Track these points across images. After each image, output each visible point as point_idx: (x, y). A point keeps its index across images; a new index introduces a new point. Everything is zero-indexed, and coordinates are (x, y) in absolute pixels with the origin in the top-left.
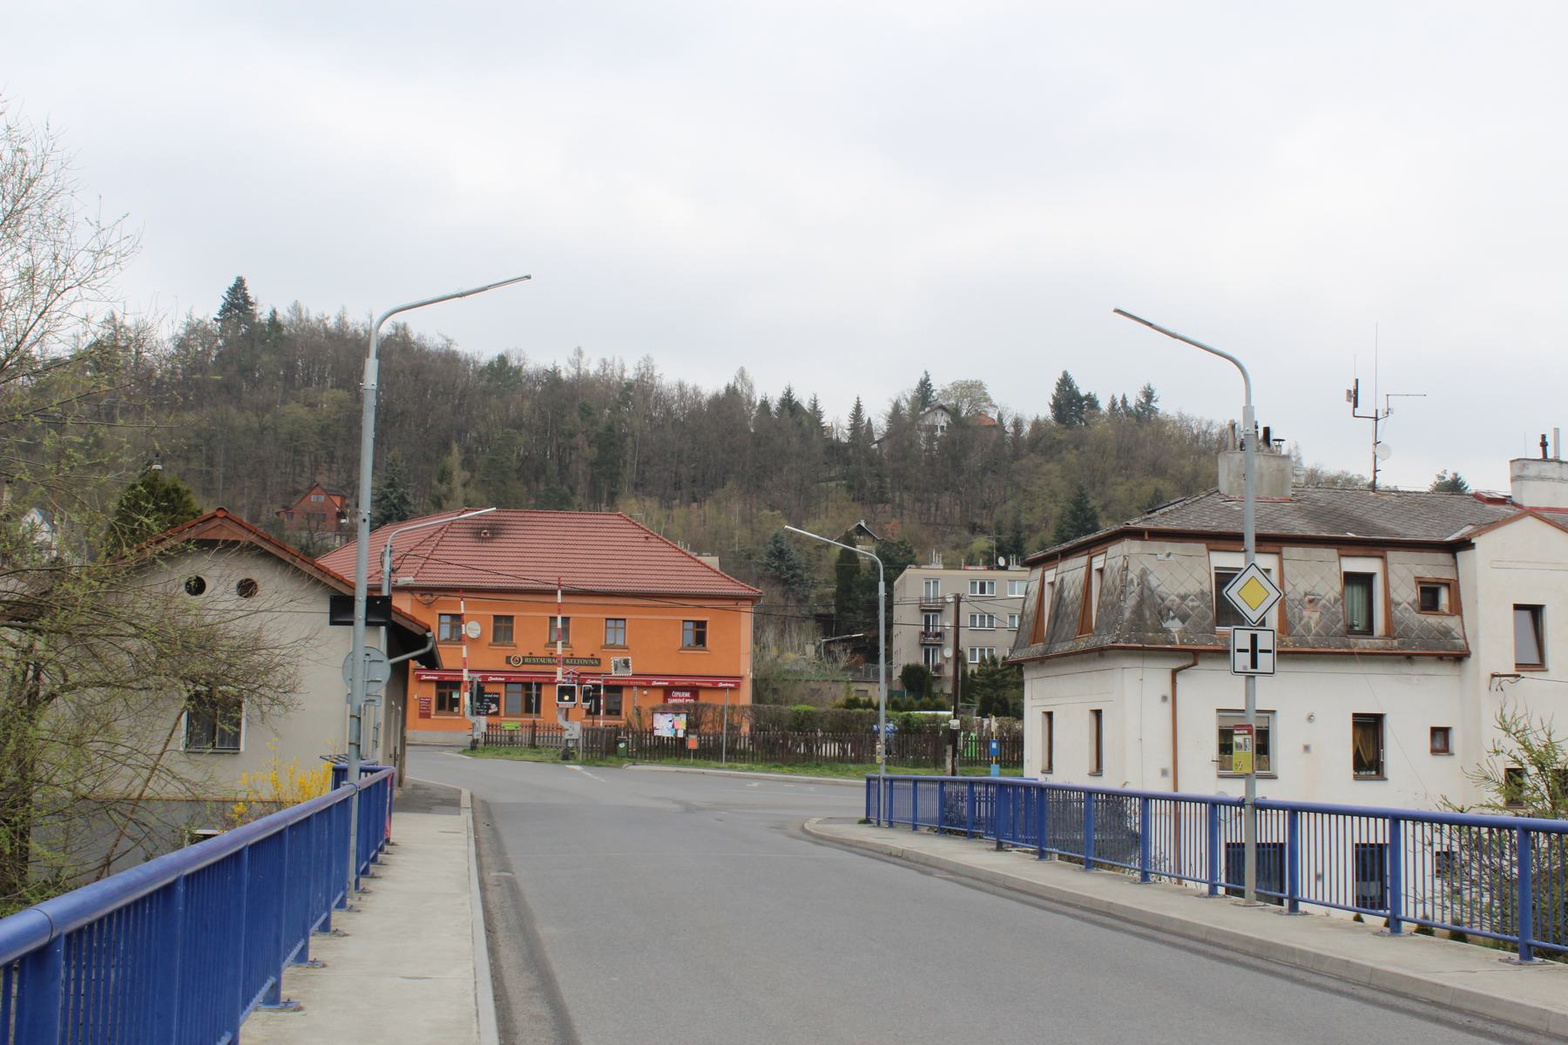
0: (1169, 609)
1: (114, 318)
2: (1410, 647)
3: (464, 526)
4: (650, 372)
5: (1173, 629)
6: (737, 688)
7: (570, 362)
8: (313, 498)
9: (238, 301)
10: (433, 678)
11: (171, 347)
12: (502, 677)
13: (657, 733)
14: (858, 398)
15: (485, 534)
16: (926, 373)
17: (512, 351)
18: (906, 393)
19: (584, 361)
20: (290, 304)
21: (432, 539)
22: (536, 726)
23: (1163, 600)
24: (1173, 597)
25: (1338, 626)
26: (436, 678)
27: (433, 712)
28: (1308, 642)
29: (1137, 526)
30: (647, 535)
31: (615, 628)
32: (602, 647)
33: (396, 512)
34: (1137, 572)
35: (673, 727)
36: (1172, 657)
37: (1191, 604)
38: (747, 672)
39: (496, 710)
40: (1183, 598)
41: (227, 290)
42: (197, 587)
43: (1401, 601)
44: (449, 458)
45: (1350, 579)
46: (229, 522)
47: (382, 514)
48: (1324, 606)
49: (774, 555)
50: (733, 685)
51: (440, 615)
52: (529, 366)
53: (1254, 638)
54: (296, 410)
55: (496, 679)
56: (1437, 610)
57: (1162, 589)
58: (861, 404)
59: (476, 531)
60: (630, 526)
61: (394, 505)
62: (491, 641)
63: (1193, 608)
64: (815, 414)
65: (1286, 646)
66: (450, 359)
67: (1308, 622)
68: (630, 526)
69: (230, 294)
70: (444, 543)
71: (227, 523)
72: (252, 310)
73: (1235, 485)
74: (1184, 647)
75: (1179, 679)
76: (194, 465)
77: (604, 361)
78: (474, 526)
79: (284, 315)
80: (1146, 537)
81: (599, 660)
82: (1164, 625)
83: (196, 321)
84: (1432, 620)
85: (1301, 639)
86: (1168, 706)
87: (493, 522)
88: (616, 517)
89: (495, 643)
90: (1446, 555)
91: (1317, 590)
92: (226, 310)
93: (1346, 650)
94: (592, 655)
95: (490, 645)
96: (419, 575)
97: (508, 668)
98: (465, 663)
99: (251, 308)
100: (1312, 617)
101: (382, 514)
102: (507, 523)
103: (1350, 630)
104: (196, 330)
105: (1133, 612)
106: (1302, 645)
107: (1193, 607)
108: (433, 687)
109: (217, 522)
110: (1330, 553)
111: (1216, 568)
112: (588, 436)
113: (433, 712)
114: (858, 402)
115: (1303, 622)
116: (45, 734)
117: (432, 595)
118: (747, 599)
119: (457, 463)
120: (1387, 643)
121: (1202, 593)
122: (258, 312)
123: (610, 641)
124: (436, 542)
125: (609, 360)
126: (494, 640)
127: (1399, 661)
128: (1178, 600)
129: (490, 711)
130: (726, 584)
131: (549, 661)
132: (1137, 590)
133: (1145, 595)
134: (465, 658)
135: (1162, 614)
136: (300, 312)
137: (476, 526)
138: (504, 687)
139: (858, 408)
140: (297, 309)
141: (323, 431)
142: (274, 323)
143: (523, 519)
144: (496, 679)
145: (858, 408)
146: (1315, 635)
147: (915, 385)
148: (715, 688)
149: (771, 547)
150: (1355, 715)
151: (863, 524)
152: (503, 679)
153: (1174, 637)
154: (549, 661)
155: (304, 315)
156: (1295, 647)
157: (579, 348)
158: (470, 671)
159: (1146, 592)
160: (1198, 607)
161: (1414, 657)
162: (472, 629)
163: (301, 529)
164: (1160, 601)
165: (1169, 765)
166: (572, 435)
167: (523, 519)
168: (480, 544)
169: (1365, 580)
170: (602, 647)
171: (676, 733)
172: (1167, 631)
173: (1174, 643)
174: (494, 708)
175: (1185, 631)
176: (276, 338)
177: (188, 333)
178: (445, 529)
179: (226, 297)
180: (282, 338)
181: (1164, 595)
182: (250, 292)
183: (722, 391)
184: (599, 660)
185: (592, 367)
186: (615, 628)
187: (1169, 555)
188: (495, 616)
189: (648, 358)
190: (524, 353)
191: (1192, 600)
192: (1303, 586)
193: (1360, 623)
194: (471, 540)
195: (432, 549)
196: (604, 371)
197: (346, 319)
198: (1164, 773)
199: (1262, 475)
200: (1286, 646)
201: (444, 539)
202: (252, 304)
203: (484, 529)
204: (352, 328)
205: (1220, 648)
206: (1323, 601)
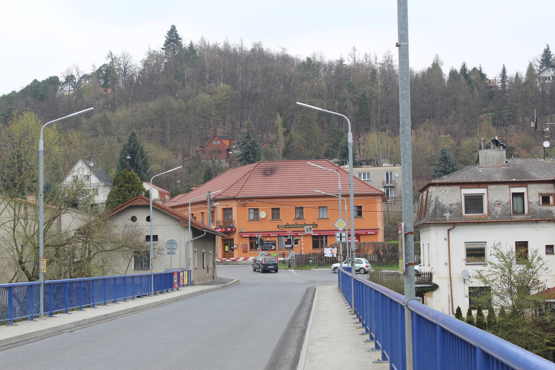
0: (446, 209)
1: (111, 54)
2: (535, 217)
3: (259, 170)
4: (390, 59)
5: (447, 216)
6: (376, 234)
7: (350, 55)
8: (214, 143)
10: (248, 236)
11: (141, 66)
12: (276, 234)
13: (325, 255)
14: (504, 65)
15: (268, 172)
16: (547, 45)
18: (538, 57)
19: (357, 54)
20: (199, 39)
21: (246, 176)
22: (285, 255)
23: (443, 206)
24: (447, 205)
26: (249, 236)
27: (248, 250)
28: (496, 218)
29: (435, 182)
30: (337, 169)
31: (323, 211)
32: (318, 219)
33: (251, 150)
34: (435, 197)
35: (332, 253)
36: (448, 225)
37: (453, 207)
38: (380, 226)
40: (451, 205)
41: (167, 32)
42: (134, 219)
43: (532, 202)
44: (276, 121)
45: (514, 195)
46: (142, 199)
47: (244, 152)
48: (503, 205)
49: (443, 160)
50: (374, 233)
51: (249, 209)
52: (326, 60)
54: (204, 97)
55: (274, 235)
56: (549, 204)
58: (506, 68)
59: (264, 171)
60: (331, 165)
61: (250, 147)
62: (271, 219)
63: (454, 209)
64: (483, 76)
65: (488, 220)
66: (285, 59)
68: (331, 165)
69: (168, 34)
70: (250, 178)
71: (142, 200)
72: (180, 42)
73: (484, 162)
74: (450, 222)
75: (450, 233)
76: (156, 128)
77: (366, 54)
78: (263, 169)
79: (196, 42)
80: (437, 185)
81: (317, 225)
82: (444, 215)
83: (153, 51)
84: (545, 208)
85: (494, 217)
86: (447, 242)
87: (272, 167)
88: (325, 161)
89: (273, 220)
90: (551, 184)
91: (501, 200)
92: (167, 43)
93: (510, 220)
94: (314, 223)
95: (270, 221)
96: (240, 193)
97: (278, 230)
99: (180, 41)
100: (499, 209)
101: (244, 152)
102: (278, 167)
103: (515, 213)
105: (433, 211)
106: (494, 219)
108: (248, 240)
109: (138, 199)
110: (507, 186)
111: (464, 194)
112: (352, 100)
113: (248, 250)
114: (504, 67)
116: (93, 266)
117: (245, 201)
118: (380, 195)
119: (280, 124)
120: (526, 217)
121: (458, 203)
123: (321, 217)
124: (247, 178)
125: (368, 54)
126: (272, 218)
127: (533, 223)
128: (449, 206)
129: (272, 249)
130: (370, 189)
131: (296, 226)
132: (435, 203)
133: (437, 205)
135: (443, 211)
137: (264, 169)
138: (277, 238)
139: (504, 71)
140: (203, 40)
141: (218, 106)
142: (191, 47)
143: (284, 165)
144: (274, 235)
145: (504, 71)
146: (499, 215)
147: (542, 52)
148: (367, 235)
149: (440, 156)
150: (516, 242)
152: (277, 235)
154: (296, 226)
155: (207, 44)
157: (354, 47)
159: (438, 204)
160: (456, 208)
161: (539, 221)
162: (263, 214)
163: (208, 159)
164: (442, 207)
165: (448, 262)
166: (344, 100)
167: (284, 165)
168: (266, 177)
169: (522, 195)
170: (318, 219)
171: (333, 255)
172: (445, 217)
173: (447, 221)
174: (273, 247)
175: (451, 216)
176: (193, 58)
177: (149, 58)
178: (251, 172)
179: (167, 36)
180: (195, 58)
181: (444, 205)
182: (178, 33)
184: (317, 225)
185: (360, 58)
186: (323, 211)
187: (446, 191)
188: (272, 208)
189: (389, 51)
191: (454, 206)
192: (495, 199)
193: (520, 209)
194: (262, 176)
195: (245, 181)
198: (446, 264)
199: (494, 157)
200: (488, 220)
201: (251, 176)
202: (180, 39)
203: (268, 170)
204: (232, 47)
205: (463, 222)
206: (503, 204)
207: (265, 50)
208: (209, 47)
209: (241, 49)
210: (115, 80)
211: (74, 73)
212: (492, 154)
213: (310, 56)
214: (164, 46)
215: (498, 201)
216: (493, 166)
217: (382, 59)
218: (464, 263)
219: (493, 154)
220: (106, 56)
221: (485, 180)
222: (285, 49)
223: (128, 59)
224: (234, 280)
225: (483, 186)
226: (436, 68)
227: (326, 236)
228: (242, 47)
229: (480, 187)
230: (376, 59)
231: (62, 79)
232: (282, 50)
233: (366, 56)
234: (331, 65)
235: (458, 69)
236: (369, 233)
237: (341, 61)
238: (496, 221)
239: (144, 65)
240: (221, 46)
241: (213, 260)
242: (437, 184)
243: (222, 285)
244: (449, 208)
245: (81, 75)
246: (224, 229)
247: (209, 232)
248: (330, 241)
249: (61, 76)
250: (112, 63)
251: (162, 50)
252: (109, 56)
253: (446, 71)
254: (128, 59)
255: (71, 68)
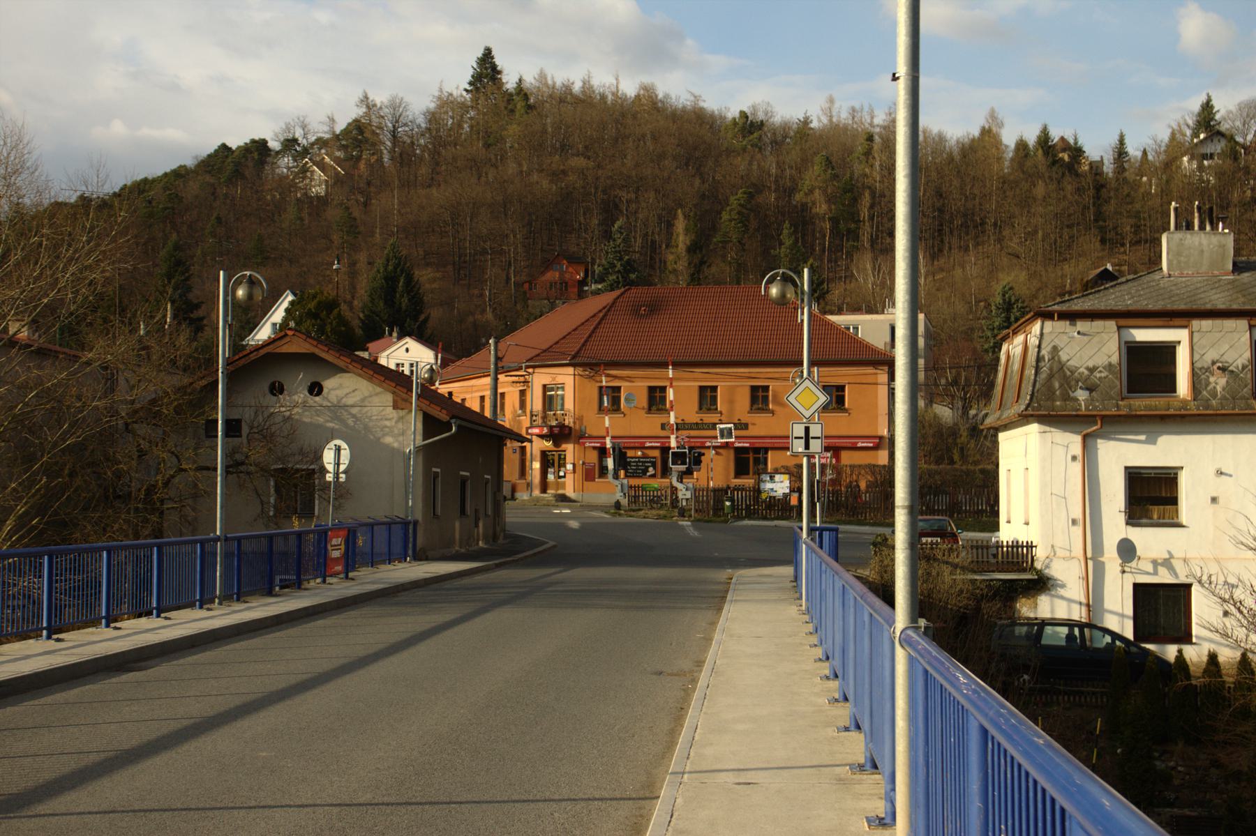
1: (367, 98)
5: (1080, 398)
9: (487, 69)
11: (421, 121)
17: (759, 104)
18: (1187, 118)
24: (1082, 370)
25: (1245, 390)
26: (598, 445)
27: (597, 476)
29: (1050, 308)
34: (1049, 349)
37: (1098, 375)
39: (654, 472)
40: (1092, 370)
52: (776, 119)
53: (807, 430)
57: (1071, 363)
63: (1100, 378)
64: (1077, 152)
67: (1215, 388)
73: (1175, 262)
79: (530, 79)
83: (446, 94)
91: (1225, 358)
92: (477, 80)
98: (608, 432)
100: (1219, 382)
104: (446, 103)
107: (1100, 378)
109: (287, 339)
113: (597, 476)
115: (1209, 388)
122: (504, 81)
128: (1086, 372)
129: (648, 474)
134: (607, 428)
136: (546, 79)
139: (1122, 141)
140: (542, 76)
148: (854, 448)
151: (1109, 267)
153: (1080, 405)
155: (550, 82)
156: (1198, 409)
158: (613, 438)
160: (1105, 378)
177: (440, 107)
179: (475, 66)
183: (976, 132)
185: (842, 115)
190: (771, 107)
191: (1101, 372)
196: (853, 118)
197: (592, 83)
199: (1202, 251)
207: (660, 96)
208: (554, 87)
209: (615, 94)
210: (375, 145)
211: (299, 134)
212: (1197, 243)
213: (745, 109)
214: (470, 83)
215: (1217, 361)
216: (1198, 273)
217: (884, 117)
218: (1122, 518)
219: (1200, 244)
220: (357, 99)
221: (1182, 307)
222: (700, 96)
223: (401, 110)
224: (545, 543)
225: (1177, 321)
226: (989, 135)
227: (766, 450)
228: (618, 91)
229: (1171, 323)
230: (872, 118)
231: (274, 145)
232: (692, 98)
233: (853, 111)
234: (785, 127)
235: (1031, 137)
236: (860, 445)
237: (806, 122)
238: (1211, 412)
239: (430, 121)
240: (577, 87)
241: (494, 494)
242: (1056, 315)
243: (497, 562)
244: (1088, 378)
245: (313, 139)
246: (545, 429)
247: (464, 424)
248: (773, 459)
249: (272, 139)
250: (367, 114)
251: (464, 93)
252: (362, 101)
253: (1009, 139)
254: (401, 110)
255: (292, 123)
